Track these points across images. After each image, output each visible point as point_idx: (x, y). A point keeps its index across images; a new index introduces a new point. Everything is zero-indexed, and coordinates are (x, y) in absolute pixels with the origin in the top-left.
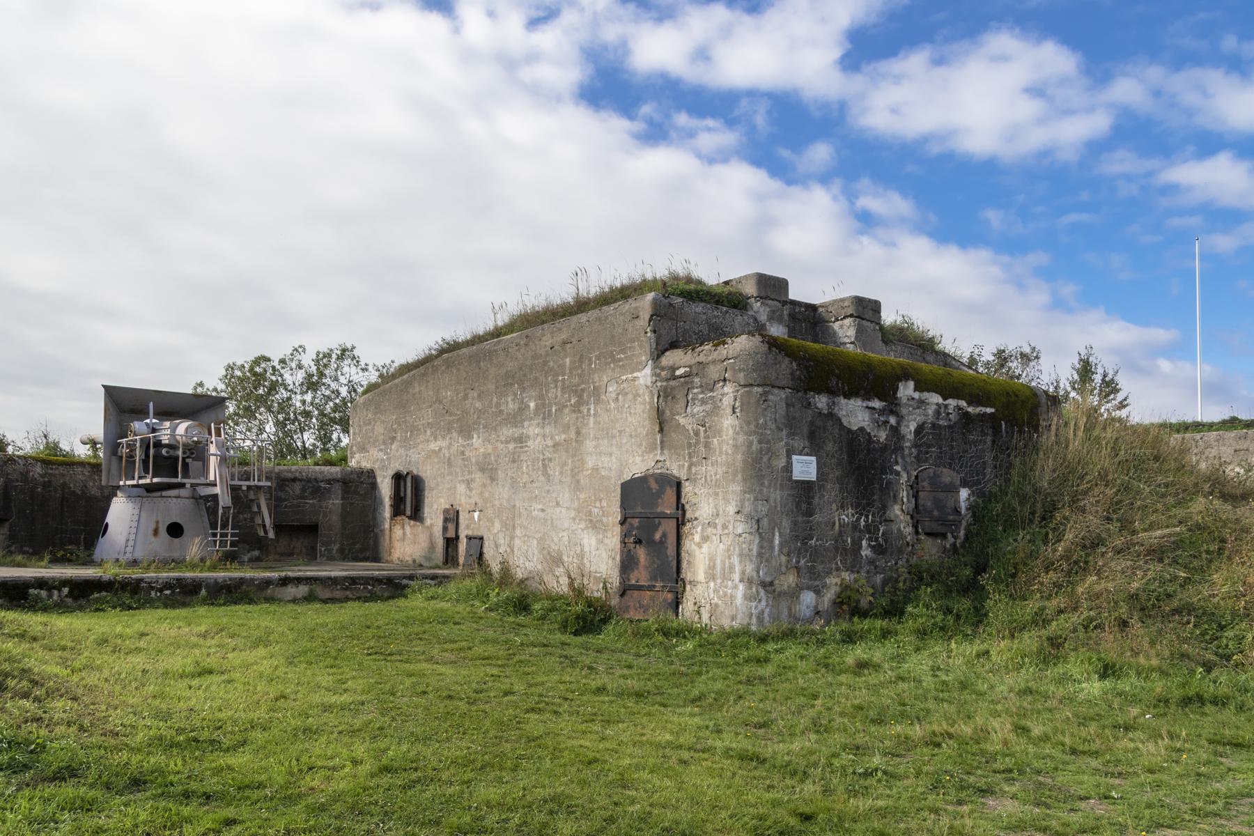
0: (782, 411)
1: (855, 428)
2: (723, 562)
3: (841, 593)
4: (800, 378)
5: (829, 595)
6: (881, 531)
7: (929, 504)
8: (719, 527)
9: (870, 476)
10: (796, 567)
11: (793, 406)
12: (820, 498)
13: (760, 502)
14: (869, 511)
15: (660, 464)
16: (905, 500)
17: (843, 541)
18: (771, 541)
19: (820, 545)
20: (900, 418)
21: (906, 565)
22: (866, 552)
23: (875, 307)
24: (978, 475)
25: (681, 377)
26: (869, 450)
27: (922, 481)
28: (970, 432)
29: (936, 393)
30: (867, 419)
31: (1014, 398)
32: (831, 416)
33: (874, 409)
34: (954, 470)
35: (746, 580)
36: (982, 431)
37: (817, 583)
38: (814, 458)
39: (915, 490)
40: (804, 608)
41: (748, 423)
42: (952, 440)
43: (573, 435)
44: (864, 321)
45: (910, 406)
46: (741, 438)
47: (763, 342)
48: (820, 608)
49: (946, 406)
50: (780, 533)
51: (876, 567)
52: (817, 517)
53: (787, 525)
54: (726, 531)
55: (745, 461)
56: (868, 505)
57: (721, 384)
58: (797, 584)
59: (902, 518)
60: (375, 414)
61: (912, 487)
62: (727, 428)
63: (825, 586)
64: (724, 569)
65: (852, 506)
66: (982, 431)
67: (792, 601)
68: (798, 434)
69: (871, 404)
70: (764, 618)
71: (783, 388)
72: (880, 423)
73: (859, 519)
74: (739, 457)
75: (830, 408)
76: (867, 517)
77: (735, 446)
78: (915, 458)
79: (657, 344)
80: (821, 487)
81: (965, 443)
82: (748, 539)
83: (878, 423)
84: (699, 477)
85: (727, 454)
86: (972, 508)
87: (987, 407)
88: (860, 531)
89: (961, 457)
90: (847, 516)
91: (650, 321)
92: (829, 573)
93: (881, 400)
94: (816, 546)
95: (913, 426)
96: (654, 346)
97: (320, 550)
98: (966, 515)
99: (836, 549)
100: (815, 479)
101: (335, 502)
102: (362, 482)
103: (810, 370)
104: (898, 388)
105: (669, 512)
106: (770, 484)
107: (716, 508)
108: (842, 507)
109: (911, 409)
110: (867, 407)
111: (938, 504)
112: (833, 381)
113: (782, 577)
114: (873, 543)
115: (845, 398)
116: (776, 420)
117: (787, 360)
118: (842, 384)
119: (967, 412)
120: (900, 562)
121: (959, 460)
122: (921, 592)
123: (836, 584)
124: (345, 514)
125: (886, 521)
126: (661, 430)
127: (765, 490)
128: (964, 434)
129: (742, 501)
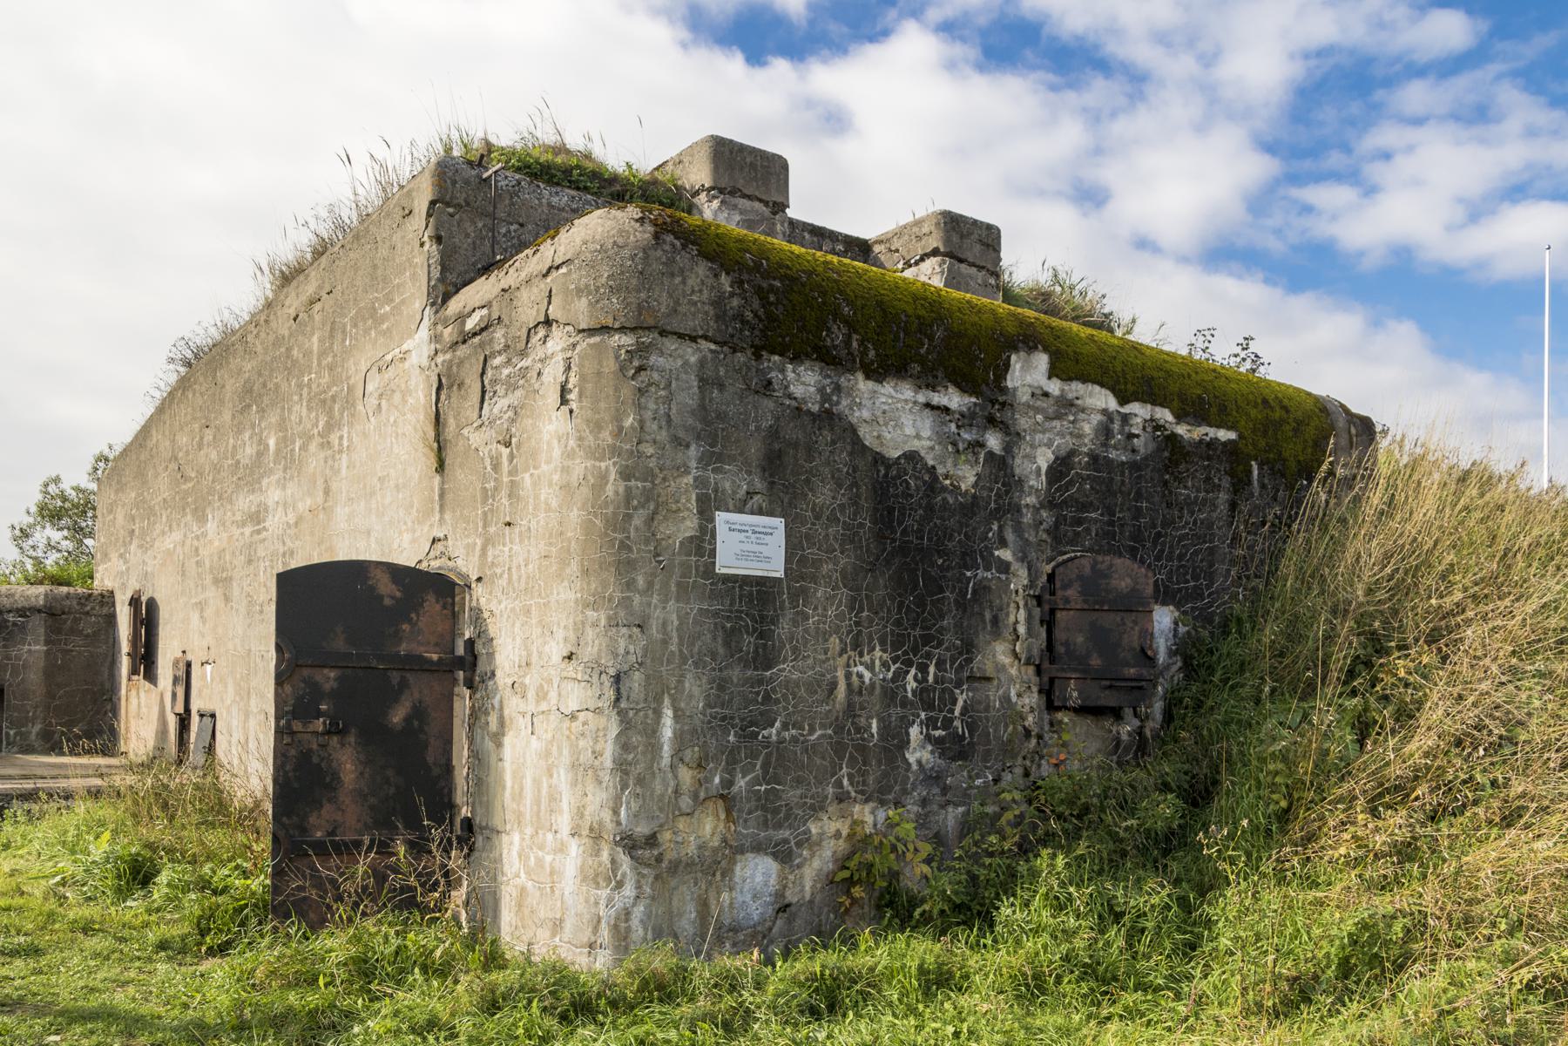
0: (688, 396)
1: (896, 454)
2: (537, 783)
3: (849, 857)
4: (739, 317)
5: (816, 863)
6: (960, 703)
7: (1080, 639)
8: (531, 694)
9: (934, 572)
10: (722, 796)
11: (721, 387)
12: (795, 623)
13: (624, 630)
14: (929, 656)
15: (439, 547)
16: (1022, 630)
17: (858, 730)
18: (653, 732)
19: (794, 740)
20: (1013, 437)
21: (1021, 781)
22: (919, 753)
23: (989, 238)
24: (1196, 578)
25: (475, 334)
26: (930, 508)
27: (1065, 587)
28: (1180, 480)
29: (1102, 385)
30: (926, 433)
31: (1278, 414)
32: (828, 417)
33: (946, 410)
34: (1142, 562)
35: (585, 832)
36: (1208, 479)
37: (785, 833)
38: (779, 523)
39: (1047, 607)
40: (748, 898)
41: (597, 427)
42: (1139, 496)
43: (320, 498)
44: (963, 266)
45: (1038, 410)
46: (580, 467)
47: (641, 220)
48: (791, 896)
49: (1125, 418)
50: (676, 710)
51: (945, 790)
52: (786, 670)
53: (696, 691)
54: (544, 706)
55: (588, 527)
56: (927, 640)
57: (541, 332)
58: (724, 840)
59: (1013, 671)
60: (117, 492)
61: (1039, 600)
62: (549, 443)
63: (805, 841)
64: (538, 802)
65: (883, 643)
66: (1208, 479)
67: (710, 883)
68: (732, 459)
69: (938, 399)
70: (628, 929)
71: (693, 339)
72: (961, 447)
73: (900, 676)
74: (575, 515)
75: (825, 398)
76: (923, 669)
77: (565, 487)
78: (1047, 531)
79: (444, 269)
80: (800, 595)
81: (1169, 505)
82: (592, 726)
83: (954, 444)
84: (498, 571)
85: (548, 509)
86: (1185, 649)
87: (1219, 427)
88: (905, 703)
89: (1159, 535)
90: (870, 667)
91: (429, 215)
92: (817, 808)
93: (963, 389)
94: (780, 742)
95: (1044, 459)
96: (436, 274)
97: (7, 734)
98: (1168, 667)
99: (839, 749)
100: (780, 574)
101: (33, 648)
102: (87, 613)
103: (772, 298)
104: (1007, 366)
105: (435, 657)
106: (650, 584)
107: (526, 648)
108: (856, 645)
109: (1039, 418)
110: (928, 405)
111: (1102, 639)
112: (838, 334)
113: (682, 824)
114: (938, 733)
115: (868, 377)
116: (669, 420)
117: (702, 269)
118: (861, 343)
119: (1174, 436)
120: (1007, 777)
121: (1155, 543)
122: (1042, 862)
123: (838, 835)
124: (50, 672)
125: (971, 678)
126: (441, 467)
127: (637, 599)
128: (1166, 483)
129: (580, 629)
